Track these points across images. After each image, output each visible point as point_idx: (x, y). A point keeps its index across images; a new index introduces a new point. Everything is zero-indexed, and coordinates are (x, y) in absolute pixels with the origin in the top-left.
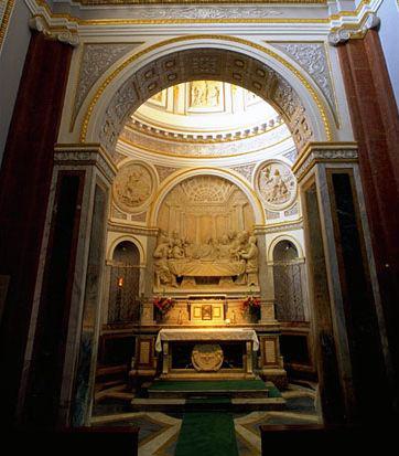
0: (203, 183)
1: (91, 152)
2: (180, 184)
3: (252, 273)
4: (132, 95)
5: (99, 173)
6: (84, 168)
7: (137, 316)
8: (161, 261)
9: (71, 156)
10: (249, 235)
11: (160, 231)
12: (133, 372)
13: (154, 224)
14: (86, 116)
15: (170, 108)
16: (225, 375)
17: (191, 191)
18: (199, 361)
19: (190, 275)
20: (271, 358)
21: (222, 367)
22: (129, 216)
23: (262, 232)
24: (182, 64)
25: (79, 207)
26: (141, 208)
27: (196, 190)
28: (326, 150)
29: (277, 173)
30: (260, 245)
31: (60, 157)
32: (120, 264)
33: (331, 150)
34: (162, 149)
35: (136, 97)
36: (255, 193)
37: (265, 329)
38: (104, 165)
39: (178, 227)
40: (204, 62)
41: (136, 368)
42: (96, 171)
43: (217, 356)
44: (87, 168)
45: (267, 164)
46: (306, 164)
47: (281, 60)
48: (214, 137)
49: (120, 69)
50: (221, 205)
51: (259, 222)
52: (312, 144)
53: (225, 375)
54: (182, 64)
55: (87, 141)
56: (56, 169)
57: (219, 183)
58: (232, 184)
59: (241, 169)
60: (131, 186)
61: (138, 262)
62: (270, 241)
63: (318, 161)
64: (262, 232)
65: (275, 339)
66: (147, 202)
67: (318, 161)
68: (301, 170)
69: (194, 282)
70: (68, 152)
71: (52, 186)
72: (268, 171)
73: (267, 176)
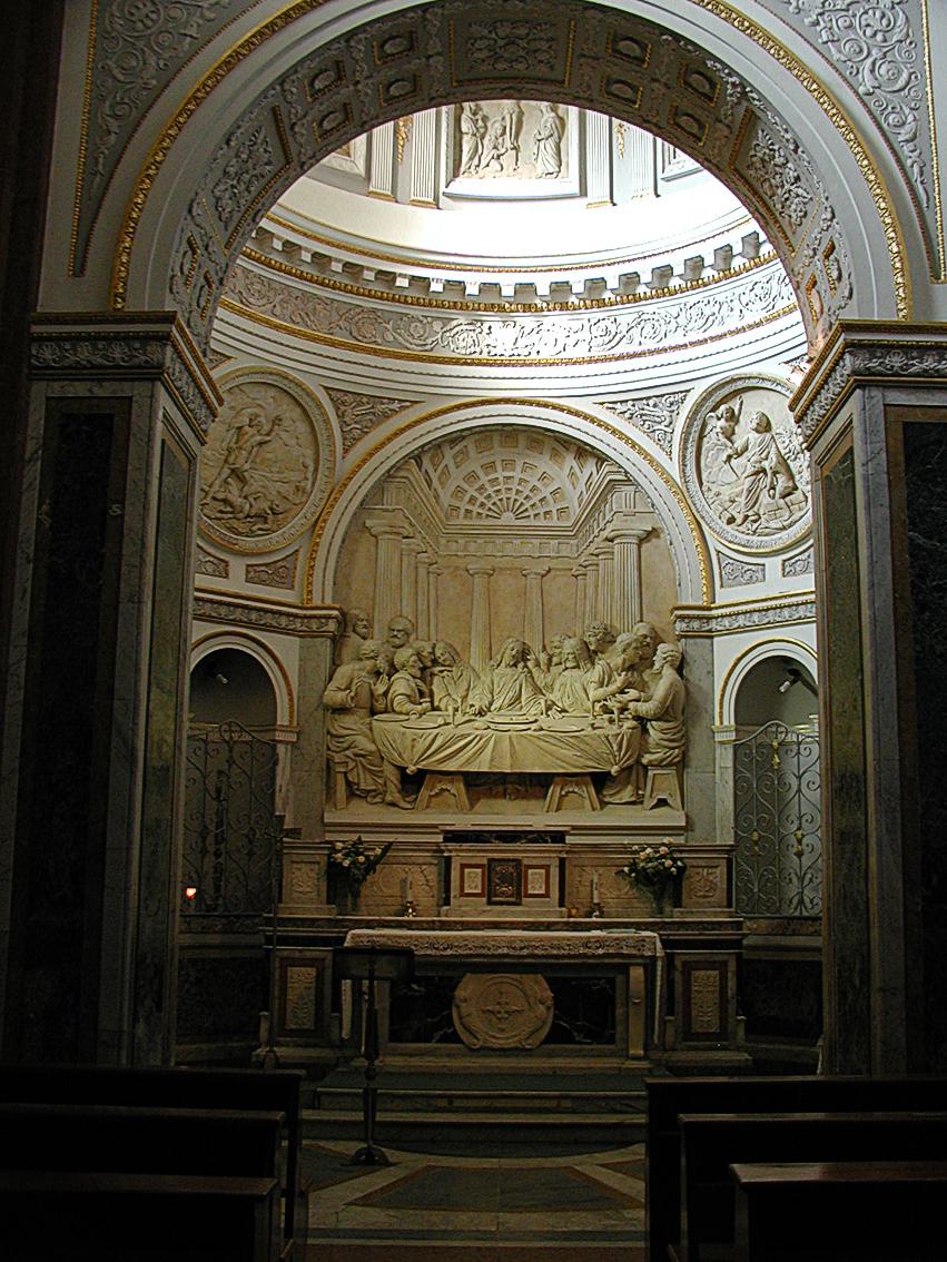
0: (498, 453)
1: (147, 338)
2: (417, 457)
3: (659, 765)
4: (268, 150)
5: (661, 457)
6: (125, 389)
7: (271, 891)
8: (348, 720)
9: (84, 353)
10: (657, 639)
11: (344, 621)
12: (262, 1051)
13: (323, 594)
14: (125, 225)
15: (381, 178)
16: (559, 1062)
17: (455, 471)
18: (477, 1023)
19: (452, 766)
20: (706, 1014)
21: (546, 1041)
22: (238, 566)
23: (701, 625)
24: (435, 45)
25: (115, 509)
26: (283, 539)
27: (472, 477)
28: (889, 348)
29: (765, 426)
30: (695, 673)
31: (48, 354)
32: (212, 730)
33: (906, 349)
34: (360, 336)
35: (278, 158)
36: (683, 496)
37: (692, 935)
38: (183, 382)
39: (407, 611)
40: (511, 41)
41: (271, 1043)
42: (164, 400)
43: (534, 1002)
44: (138, 390)
45: (730, 392)
46: (832, 389)
47: (768, 41)
48: (543, 289)
49: (229, 64)
50: (561, 536)
51: (692, 596)
52: (847, 327)
53: (559, 1062)
54: (435, 45)
55: (132, 306)
56: (39, 393)
57: (555, 454)
58: (601, 459)
59: (639, 406)
60: (241, 461)
61: (271, 725)
62: (729, 658)
63: (863, 381)
64: (701, 625)
65: (722, 966)
66: (297, 523)
67: (863, 380)
68: (817, 411)
69: (459, 788)
70: (76, 339)
71: (31, 446)
72: (733, 417)
73: (729, 435)
